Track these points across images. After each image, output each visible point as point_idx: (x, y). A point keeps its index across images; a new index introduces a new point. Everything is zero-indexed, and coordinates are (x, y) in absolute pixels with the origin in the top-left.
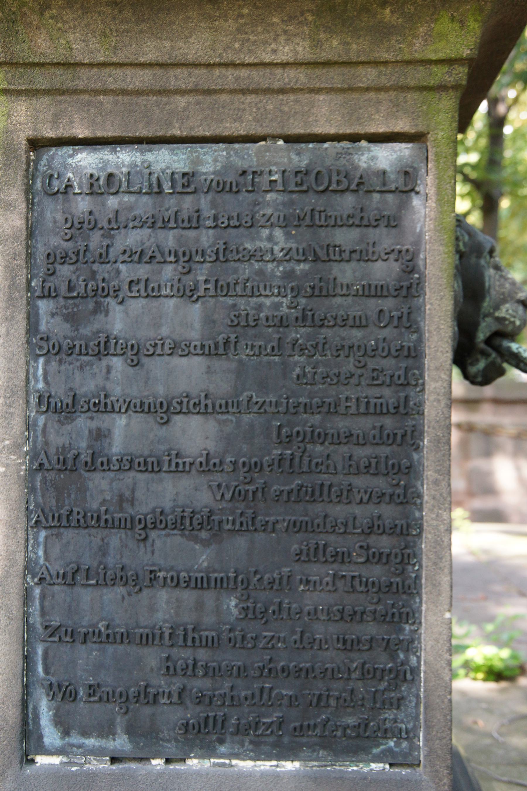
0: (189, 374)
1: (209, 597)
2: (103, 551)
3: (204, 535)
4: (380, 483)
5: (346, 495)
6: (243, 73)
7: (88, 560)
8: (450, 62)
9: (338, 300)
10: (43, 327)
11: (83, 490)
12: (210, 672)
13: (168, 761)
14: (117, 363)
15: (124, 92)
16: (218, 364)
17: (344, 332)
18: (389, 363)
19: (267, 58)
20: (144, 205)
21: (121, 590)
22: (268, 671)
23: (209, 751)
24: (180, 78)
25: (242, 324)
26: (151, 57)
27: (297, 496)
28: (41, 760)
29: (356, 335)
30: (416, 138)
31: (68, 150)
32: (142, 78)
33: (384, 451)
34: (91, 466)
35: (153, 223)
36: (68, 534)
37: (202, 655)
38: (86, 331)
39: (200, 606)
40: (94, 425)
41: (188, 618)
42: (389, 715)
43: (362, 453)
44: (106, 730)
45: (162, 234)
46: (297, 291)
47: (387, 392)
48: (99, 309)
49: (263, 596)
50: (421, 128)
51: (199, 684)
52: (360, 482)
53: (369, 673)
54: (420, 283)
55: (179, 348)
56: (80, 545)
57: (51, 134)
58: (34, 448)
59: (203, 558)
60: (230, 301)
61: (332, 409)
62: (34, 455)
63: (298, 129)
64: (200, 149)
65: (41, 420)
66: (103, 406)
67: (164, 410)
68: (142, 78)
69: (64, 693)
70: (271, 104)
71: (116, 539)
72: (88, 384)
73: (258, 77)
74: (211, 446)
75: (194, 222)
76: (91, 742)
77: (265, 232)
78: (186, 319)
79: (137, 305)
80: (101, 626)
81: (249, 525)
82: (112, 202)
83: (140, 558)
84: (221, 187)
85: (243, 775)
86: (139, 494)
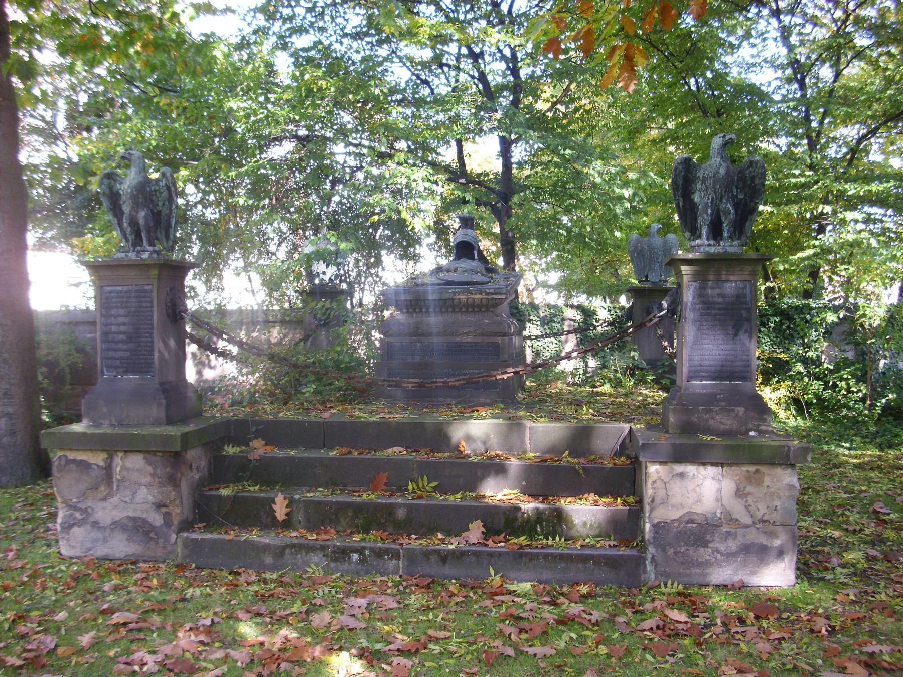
0: (121, 320)
35: (117, 298)
55: (121, 316)
59: (125, 347)
66: (111, 325)
67: (119, 325)
69: (107, 367)
78: (122, 312)
84: (126, 292)
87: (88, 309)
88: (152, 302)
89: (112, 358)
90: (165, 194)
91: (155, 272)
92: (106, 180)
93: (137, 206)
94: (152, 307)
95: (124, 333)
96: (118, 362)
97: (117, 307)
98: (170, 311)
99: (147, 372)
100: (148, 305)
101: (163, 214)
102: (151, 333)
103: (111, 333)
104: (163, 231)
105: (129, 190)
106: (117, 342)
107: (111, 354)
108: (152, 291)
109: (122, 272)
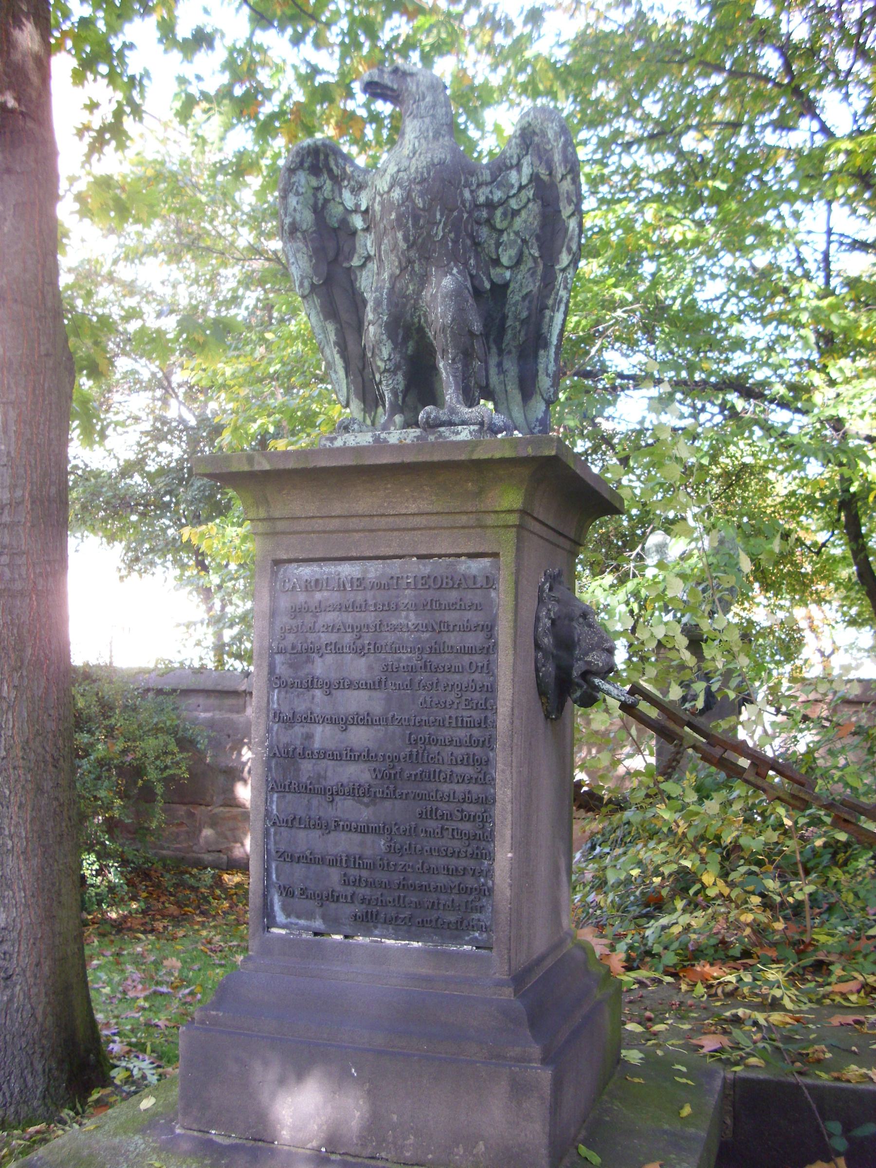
0: (355, 701)
1: (369, 838)
2: (309, 807)
3: (366, 800)
4: (470, 771)
5: (449, 778)
6: (391, 519)
7: (301, 813)
8: (510, 511)
9: (446, 656)
10: (278, 671)
11: (297, 770)
12: (370, 884)
13: (346, 937)
14: (318, 693)
15: (325, 532)
16: (377, 694)
17: (449, 676)
18: (477, 695)
19: (404, 511)
20: (335, 597)
21: (318, 833)
22: (402, 886)
23: (367, 933)
24: (353, 523)
25: (389, 669)
26: (339, 512)
27: (421, 778)
28: (274, 930)
29: (456, 678)
30: (495, 555)
31: (295, 565)
32: (335, 524)
33: (476, 750)
34: (303, 756)
35: (341, 608)
36: (289, 797)
37: (365, 873)
38: (301, 674)
39: (362, 844)
40: (304, 730)
41: (356, 850)
42: (476, 916)
43: (460, 751)
44: (310, 916)
45: (345, 615)
46: (421, 650)
47: (474, 713)
48: (309, 661)
49: (399, 839)
50: (496, 550)
51: (362, 891)
52: (459, 769)
53: (464, 890)
54: (495, 644)
55: (353, 685)
56: (297, 804)
57: (285, 557)
58: (271, 742)
59: (365, 814)
60: (383, 656)
61: (441, 724)
62: (271, 747)
63: (423, 551)
64: (368, 563)
65: (276, 727)
66: (309, 719)
67: (344, 722)
68: (335, 524)
69: (287, 892)
70: (407, 536)
71: (316, 800)
72: (301, 707)
73: (399, 522)
74: (370, 745)
75: (363, 607)
76: (302, 922)
77: (404, 614)
78: (358, 667)
79: (330, 658)
80: (308, 853)
81: (392, 795)
82: (318, 596)
83: (330, 812)
84: (379, 586)
85: (388, 948)
86: (329, 774)
87: (203, 667)
88: (489, 629)
89: (311, 859)
90: (528, 219)
91: (509, 498)
92: (302, 177)
93: (426, 258)
94: (489, 650)
95: (367, 756)
96: (334, 875)
97: (337, 649)
98: (550, 669)
99: (458, 930)
100: (474, 639)
101: (514, 297)
102: (485, 763)
103: (306, 753)
104: (511, 366)
105: (397, 194)
106: (332, 794)
107: (305, 840)
108: (490, 582)
109: (364, 501)
